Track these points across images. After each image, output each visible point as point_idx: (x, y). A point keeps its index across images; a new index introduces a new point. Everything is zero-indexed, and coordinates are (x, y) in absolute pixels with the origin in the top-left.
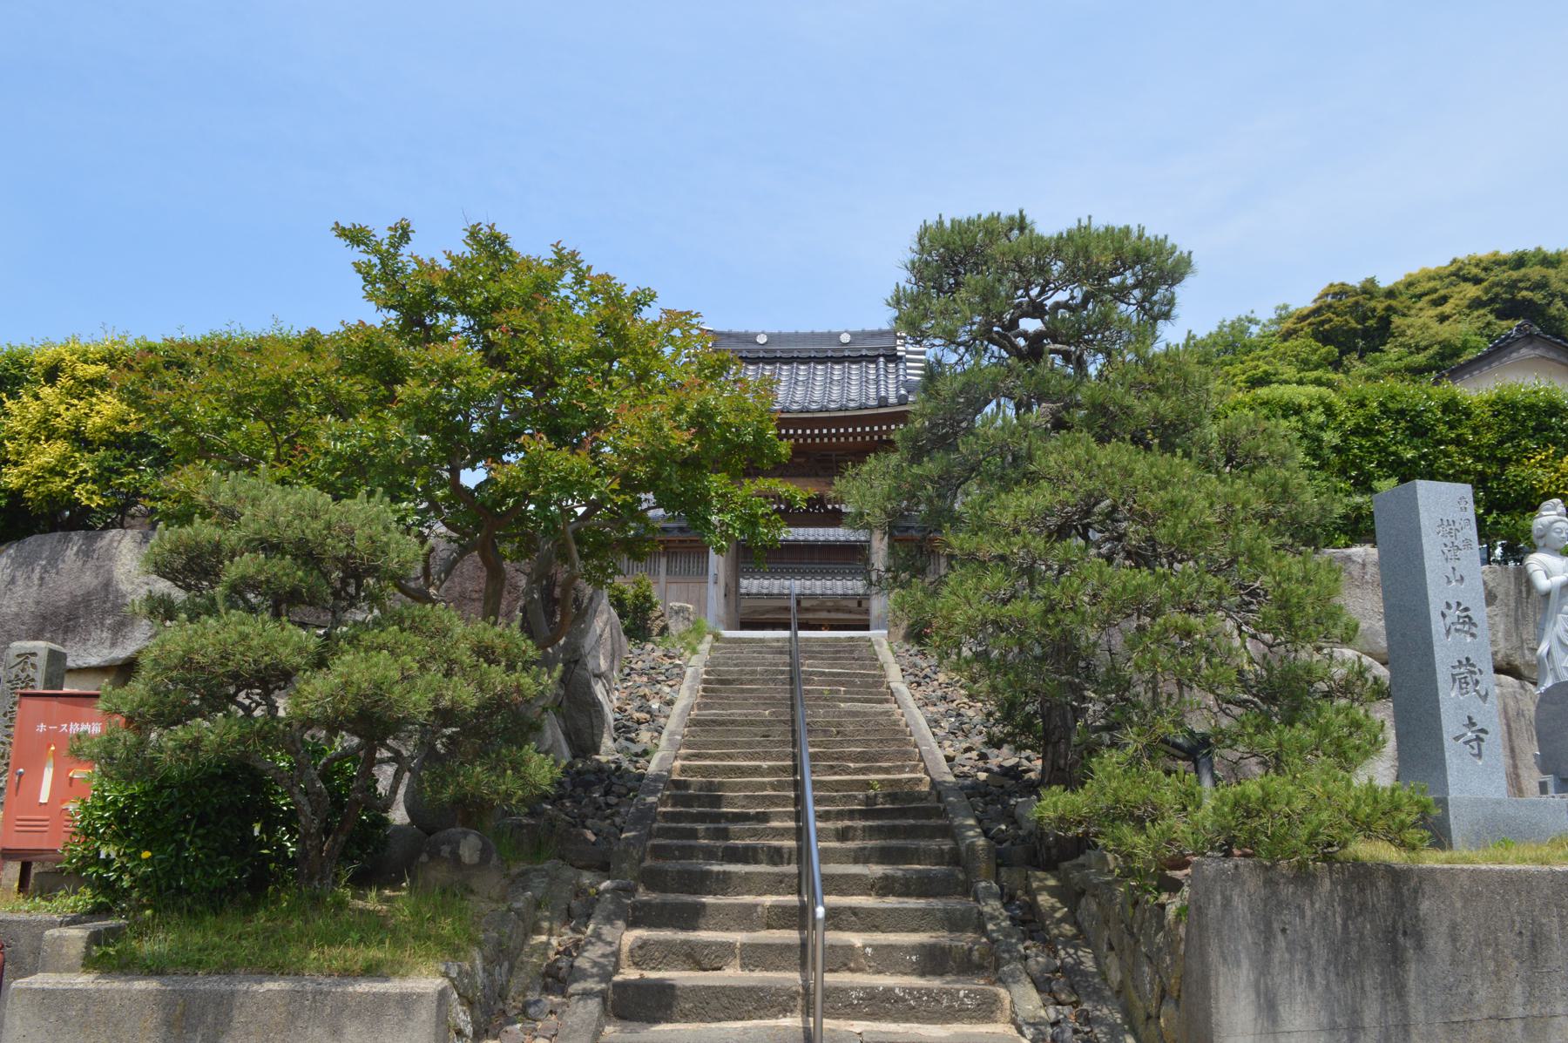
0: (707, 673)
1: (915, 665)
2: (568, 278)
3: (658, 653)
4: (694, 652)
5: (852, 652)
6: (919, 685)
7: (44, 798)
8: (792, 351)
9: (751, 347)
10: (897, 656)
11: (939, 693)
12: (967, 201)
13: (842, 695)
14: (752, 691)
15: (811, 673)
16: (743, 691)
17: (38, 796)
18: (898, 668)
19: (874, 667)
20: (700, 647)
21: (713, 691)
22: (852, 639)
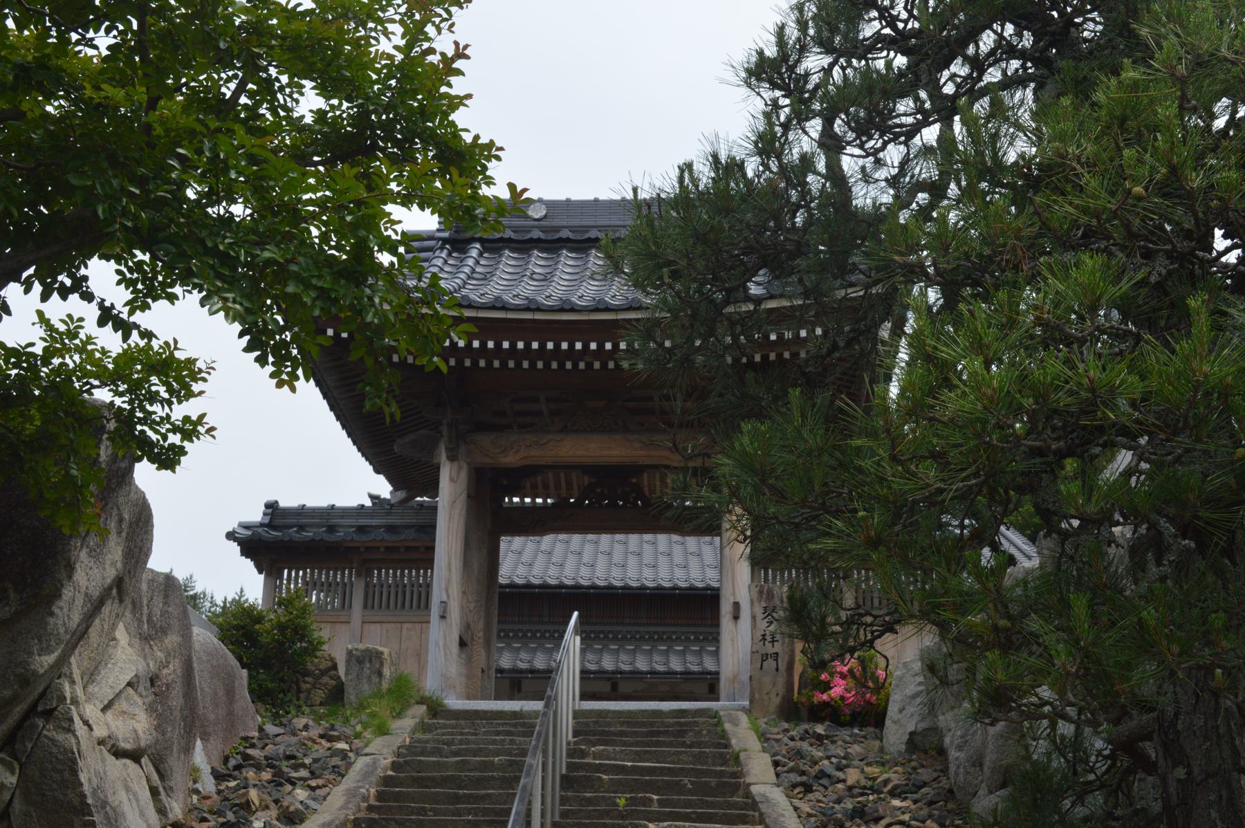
0: (395, 766)
1: (799, 754)
2: (68, 282)
3: (314, 732)
4: (382, 731)
5: (682, 733)
6: (808, 789)
7: (576, 614)
8: (587, 228)
9: (517, 222)
10: (763, 737)
11: (849, 804)
12: (166, 473)
13: (655, 808)
14: (478, 799)
15: (599, 768)
16: (457, 799)
17: (580, 616)
18: (767, 759)
19: (724, 760)
20: (395, 725)
21: (397, 797)
22: (682, 713)
